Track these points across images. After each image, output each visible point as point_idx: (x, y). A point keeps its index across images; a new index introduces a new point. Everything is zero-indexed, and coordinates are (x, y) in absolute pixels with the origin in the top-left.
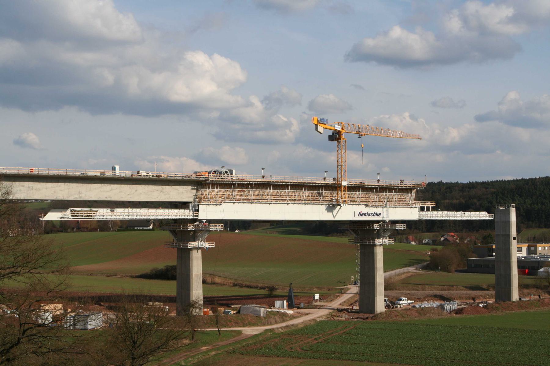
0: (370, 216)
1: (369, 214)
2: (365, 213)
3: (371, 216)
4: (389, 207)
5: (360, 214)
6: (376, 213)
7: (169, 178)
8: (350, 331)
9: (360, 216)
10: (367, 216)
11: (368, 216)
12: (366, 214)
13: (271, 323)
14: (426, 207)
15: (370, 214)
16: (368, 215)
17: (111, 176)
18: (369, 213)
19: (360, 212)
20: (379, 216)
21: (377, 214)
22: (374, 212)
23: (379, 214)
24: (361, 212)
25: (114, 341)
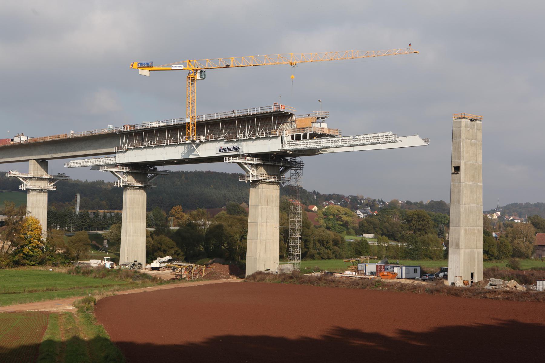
1: (229, 149)
2: (225, 149)
3: (231, 151)
4: (244, 140)
5: (221, 150)
6: (235, 147)
8: (118, 229)
9: (221, 152)
11: (228, 151)
12: (226, 149)
13: (340, 256)
15: (230, 149)
16: (228, 150)
19: (220, 148)
21: (236, 149)
22: (234, 146)
24: (222, 147)
25: (68, 203)
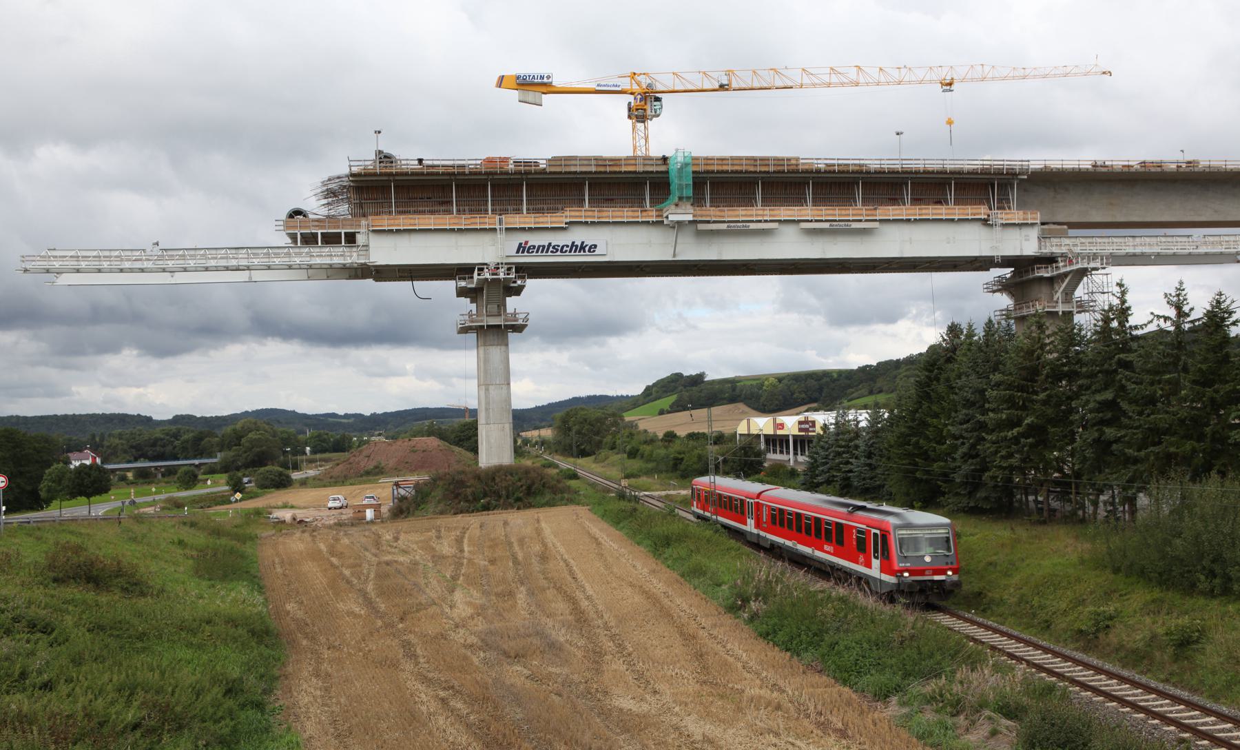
0: (559, 253)
1: (554, 247)
2: (539, 246)
7: (560, 206)
10: (547, 252)
11: (552, 252)
12: (544, 247)
14: (345, 233)
15: (559, 248)
16: (551, 249)
17: (1132, 170)
18: (553, 244)
19: (520, 244)
20: (589, 251)
23: (590, 248)
